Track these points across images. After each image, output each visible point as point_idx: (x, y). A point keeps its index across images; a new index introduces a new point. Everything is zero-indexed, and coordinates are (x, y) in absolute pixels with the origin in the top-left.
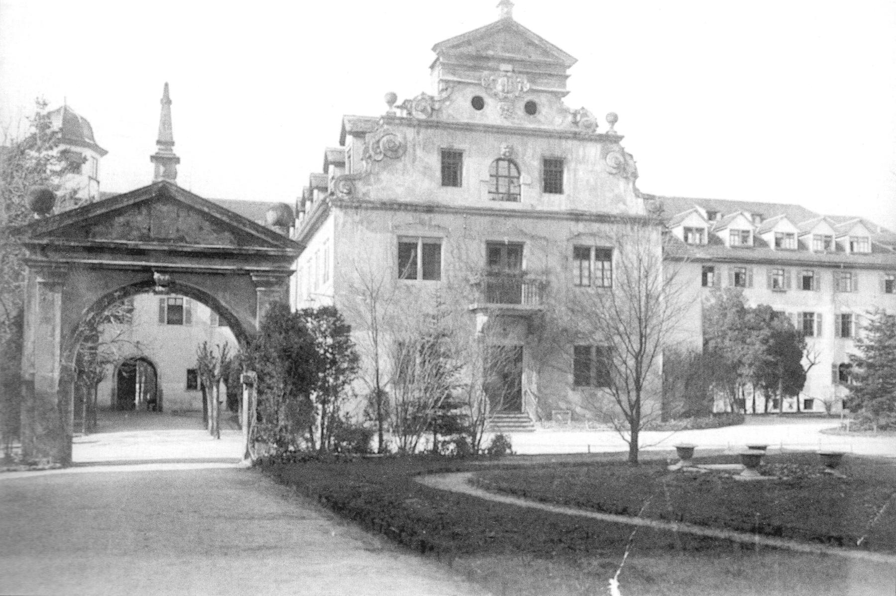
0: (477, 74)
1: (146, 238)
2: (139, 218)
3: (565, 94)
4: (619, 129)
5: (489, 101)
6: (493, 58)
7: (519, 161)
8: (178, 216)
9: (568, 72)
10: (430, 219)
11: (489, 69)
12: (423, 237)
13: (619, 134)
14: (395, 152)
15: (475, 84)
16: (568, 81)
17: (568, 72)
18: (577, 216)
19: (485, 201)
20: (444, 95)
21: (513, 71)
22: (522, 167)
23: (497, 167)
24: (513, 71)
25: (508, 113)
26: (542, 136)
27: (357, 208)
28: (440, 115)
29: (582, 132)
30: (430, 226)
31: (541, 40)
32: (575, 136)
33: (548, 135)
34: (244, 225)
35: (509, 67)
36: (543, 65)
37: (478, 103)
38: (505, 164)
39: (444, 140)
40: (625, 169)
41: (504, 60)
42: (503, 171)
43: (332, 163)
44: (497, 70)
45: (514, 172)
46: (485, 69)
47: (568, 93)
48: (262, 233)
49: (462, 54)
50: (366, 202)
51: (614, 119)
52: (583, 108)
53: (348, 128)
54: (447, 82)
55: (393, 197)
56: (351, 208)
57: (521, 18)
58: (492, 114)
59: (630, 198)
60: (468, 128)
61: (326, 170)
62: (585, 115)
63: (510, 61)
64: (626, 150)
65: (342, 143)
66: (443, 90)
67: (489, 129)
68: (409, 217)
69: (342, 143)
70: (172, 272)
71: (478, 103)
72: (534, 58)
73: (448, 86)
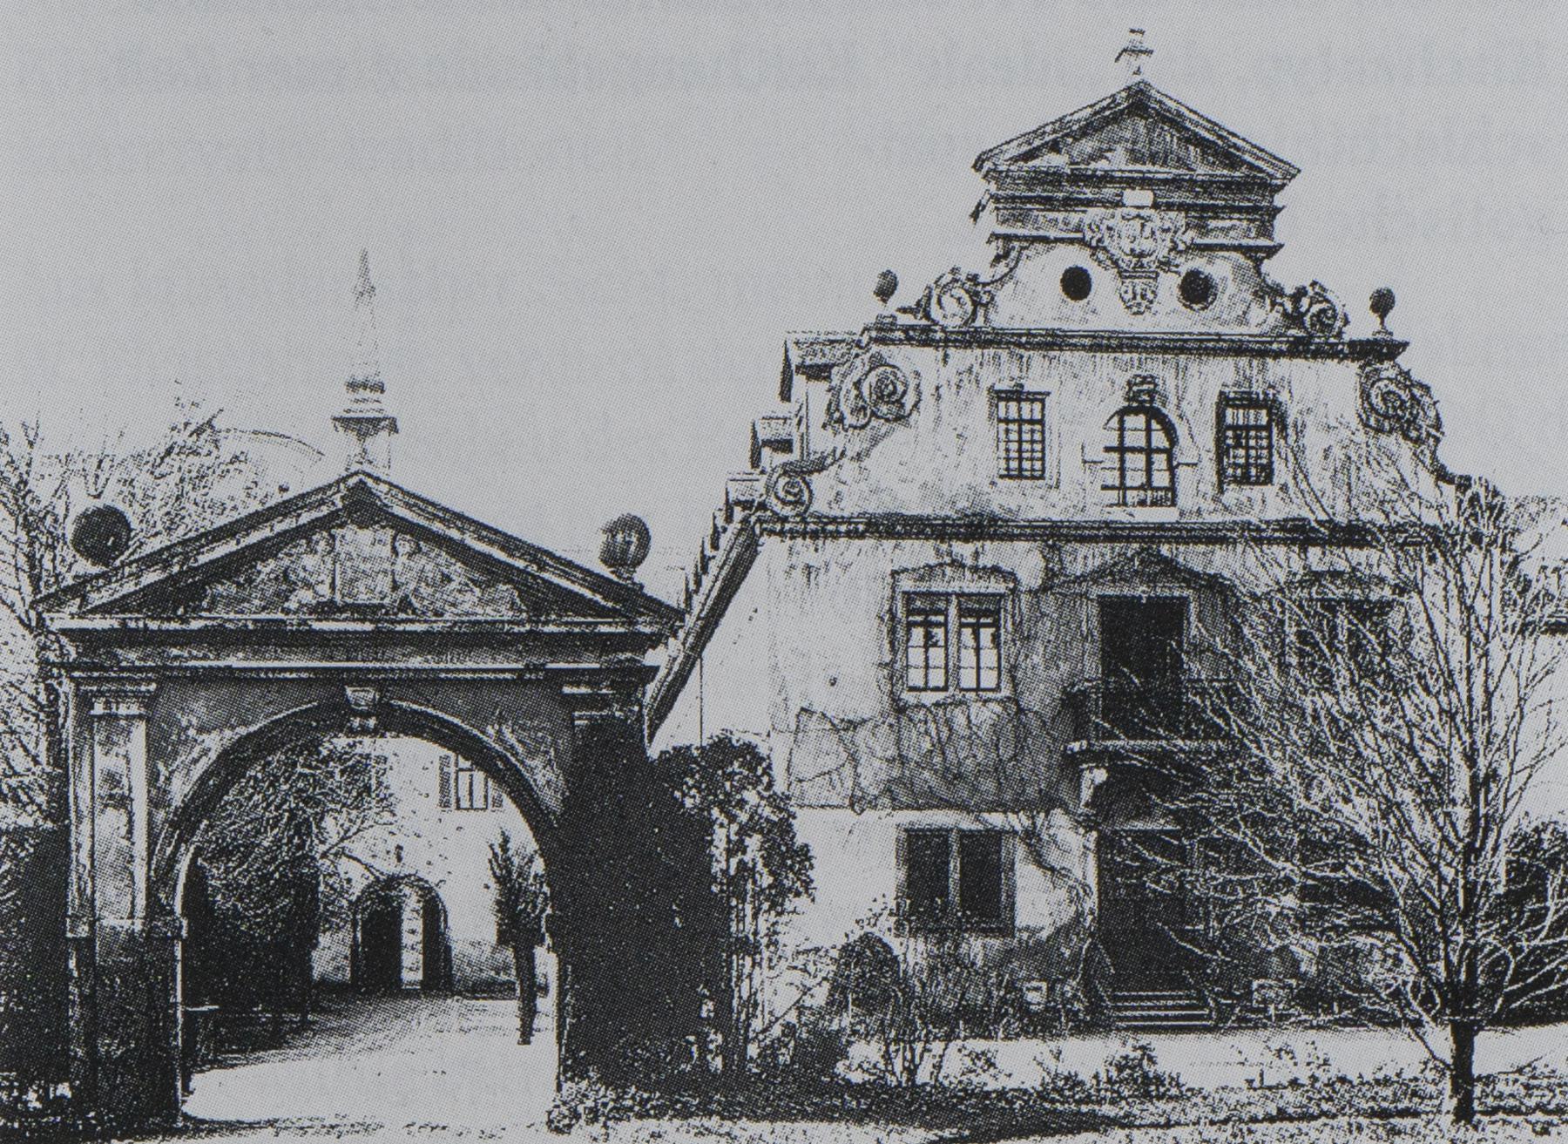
0: (1074, 218)
1: (326, 609)
2: (309, 561)
3: (1271, 251)
4: (1398, 324)
5: (1103, 281)
6: (1107, 178)
7: (1170, 412)
8: (395, 551)
9: (1278, 200)
10: (976, 554)
11: (1104, 203)
12: (958, 595)
13: (1398, 337)
14: (889, 404)
15: (1071, 241)
16: (1279, 222)
17: (1278, 200)
18: (1298, 534)
19: (1098, 507)
20: (1002, 268)
21: (1156, 206)
22: (1181, 430)
23: (1122, 429)
24: (1156, 206)
25: (1139, 304)
26: (1215, 352)
27: (815, 535)
28: (992, 316)
29: (1310, 331)
30: (975, 569)
31: (1214, 126)
32: (1298, 349)
33: (1237, 349)
34: (542, 567)
35: (1146, 197)
36: (1234, 186)
37: (1076, 284)
38: (1139, 421)
39: (1001, 371)
40: (1402, 414)
41: (1131, 183)
42: (1135, 439)
43: (767, 443)
44: (1119, 204)
45: (1159, 439)
46: (1089, 203)
47: (1281, 246)
48: (491, 543)
49: (1036, 171)
50: (834, 520)
51: (1382, 303)
52: (1314, 284)
53: (795, 361)
54: (1007, 238)
55: (892, 508)
56: (804, 535)
57: (1173, 84)
58: (1106, 308)
59: (1425, 483)
60: (1053, 342)
61: (755, 460)
62: (1321, 296)
63: (1144, 182)
64: (1415, 376)
65: (785, 395)
66: (998, 259)
67: (1101, 343)
68: (920, 552)
69: (785, 395)
70: (384, 682)
71: (1076, 284)
72: (1202, 171)
73: (1008, 249)
